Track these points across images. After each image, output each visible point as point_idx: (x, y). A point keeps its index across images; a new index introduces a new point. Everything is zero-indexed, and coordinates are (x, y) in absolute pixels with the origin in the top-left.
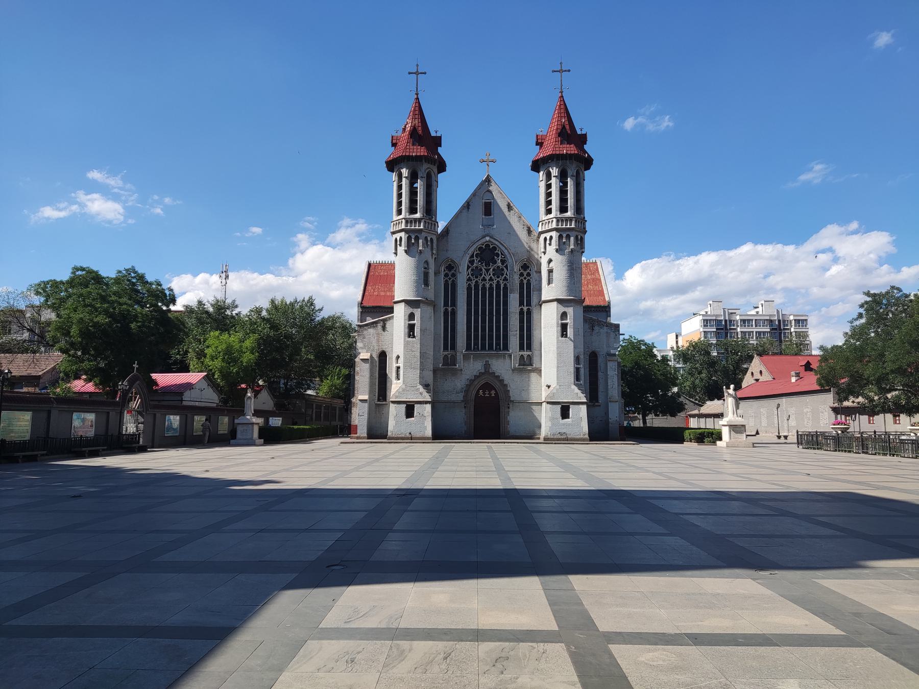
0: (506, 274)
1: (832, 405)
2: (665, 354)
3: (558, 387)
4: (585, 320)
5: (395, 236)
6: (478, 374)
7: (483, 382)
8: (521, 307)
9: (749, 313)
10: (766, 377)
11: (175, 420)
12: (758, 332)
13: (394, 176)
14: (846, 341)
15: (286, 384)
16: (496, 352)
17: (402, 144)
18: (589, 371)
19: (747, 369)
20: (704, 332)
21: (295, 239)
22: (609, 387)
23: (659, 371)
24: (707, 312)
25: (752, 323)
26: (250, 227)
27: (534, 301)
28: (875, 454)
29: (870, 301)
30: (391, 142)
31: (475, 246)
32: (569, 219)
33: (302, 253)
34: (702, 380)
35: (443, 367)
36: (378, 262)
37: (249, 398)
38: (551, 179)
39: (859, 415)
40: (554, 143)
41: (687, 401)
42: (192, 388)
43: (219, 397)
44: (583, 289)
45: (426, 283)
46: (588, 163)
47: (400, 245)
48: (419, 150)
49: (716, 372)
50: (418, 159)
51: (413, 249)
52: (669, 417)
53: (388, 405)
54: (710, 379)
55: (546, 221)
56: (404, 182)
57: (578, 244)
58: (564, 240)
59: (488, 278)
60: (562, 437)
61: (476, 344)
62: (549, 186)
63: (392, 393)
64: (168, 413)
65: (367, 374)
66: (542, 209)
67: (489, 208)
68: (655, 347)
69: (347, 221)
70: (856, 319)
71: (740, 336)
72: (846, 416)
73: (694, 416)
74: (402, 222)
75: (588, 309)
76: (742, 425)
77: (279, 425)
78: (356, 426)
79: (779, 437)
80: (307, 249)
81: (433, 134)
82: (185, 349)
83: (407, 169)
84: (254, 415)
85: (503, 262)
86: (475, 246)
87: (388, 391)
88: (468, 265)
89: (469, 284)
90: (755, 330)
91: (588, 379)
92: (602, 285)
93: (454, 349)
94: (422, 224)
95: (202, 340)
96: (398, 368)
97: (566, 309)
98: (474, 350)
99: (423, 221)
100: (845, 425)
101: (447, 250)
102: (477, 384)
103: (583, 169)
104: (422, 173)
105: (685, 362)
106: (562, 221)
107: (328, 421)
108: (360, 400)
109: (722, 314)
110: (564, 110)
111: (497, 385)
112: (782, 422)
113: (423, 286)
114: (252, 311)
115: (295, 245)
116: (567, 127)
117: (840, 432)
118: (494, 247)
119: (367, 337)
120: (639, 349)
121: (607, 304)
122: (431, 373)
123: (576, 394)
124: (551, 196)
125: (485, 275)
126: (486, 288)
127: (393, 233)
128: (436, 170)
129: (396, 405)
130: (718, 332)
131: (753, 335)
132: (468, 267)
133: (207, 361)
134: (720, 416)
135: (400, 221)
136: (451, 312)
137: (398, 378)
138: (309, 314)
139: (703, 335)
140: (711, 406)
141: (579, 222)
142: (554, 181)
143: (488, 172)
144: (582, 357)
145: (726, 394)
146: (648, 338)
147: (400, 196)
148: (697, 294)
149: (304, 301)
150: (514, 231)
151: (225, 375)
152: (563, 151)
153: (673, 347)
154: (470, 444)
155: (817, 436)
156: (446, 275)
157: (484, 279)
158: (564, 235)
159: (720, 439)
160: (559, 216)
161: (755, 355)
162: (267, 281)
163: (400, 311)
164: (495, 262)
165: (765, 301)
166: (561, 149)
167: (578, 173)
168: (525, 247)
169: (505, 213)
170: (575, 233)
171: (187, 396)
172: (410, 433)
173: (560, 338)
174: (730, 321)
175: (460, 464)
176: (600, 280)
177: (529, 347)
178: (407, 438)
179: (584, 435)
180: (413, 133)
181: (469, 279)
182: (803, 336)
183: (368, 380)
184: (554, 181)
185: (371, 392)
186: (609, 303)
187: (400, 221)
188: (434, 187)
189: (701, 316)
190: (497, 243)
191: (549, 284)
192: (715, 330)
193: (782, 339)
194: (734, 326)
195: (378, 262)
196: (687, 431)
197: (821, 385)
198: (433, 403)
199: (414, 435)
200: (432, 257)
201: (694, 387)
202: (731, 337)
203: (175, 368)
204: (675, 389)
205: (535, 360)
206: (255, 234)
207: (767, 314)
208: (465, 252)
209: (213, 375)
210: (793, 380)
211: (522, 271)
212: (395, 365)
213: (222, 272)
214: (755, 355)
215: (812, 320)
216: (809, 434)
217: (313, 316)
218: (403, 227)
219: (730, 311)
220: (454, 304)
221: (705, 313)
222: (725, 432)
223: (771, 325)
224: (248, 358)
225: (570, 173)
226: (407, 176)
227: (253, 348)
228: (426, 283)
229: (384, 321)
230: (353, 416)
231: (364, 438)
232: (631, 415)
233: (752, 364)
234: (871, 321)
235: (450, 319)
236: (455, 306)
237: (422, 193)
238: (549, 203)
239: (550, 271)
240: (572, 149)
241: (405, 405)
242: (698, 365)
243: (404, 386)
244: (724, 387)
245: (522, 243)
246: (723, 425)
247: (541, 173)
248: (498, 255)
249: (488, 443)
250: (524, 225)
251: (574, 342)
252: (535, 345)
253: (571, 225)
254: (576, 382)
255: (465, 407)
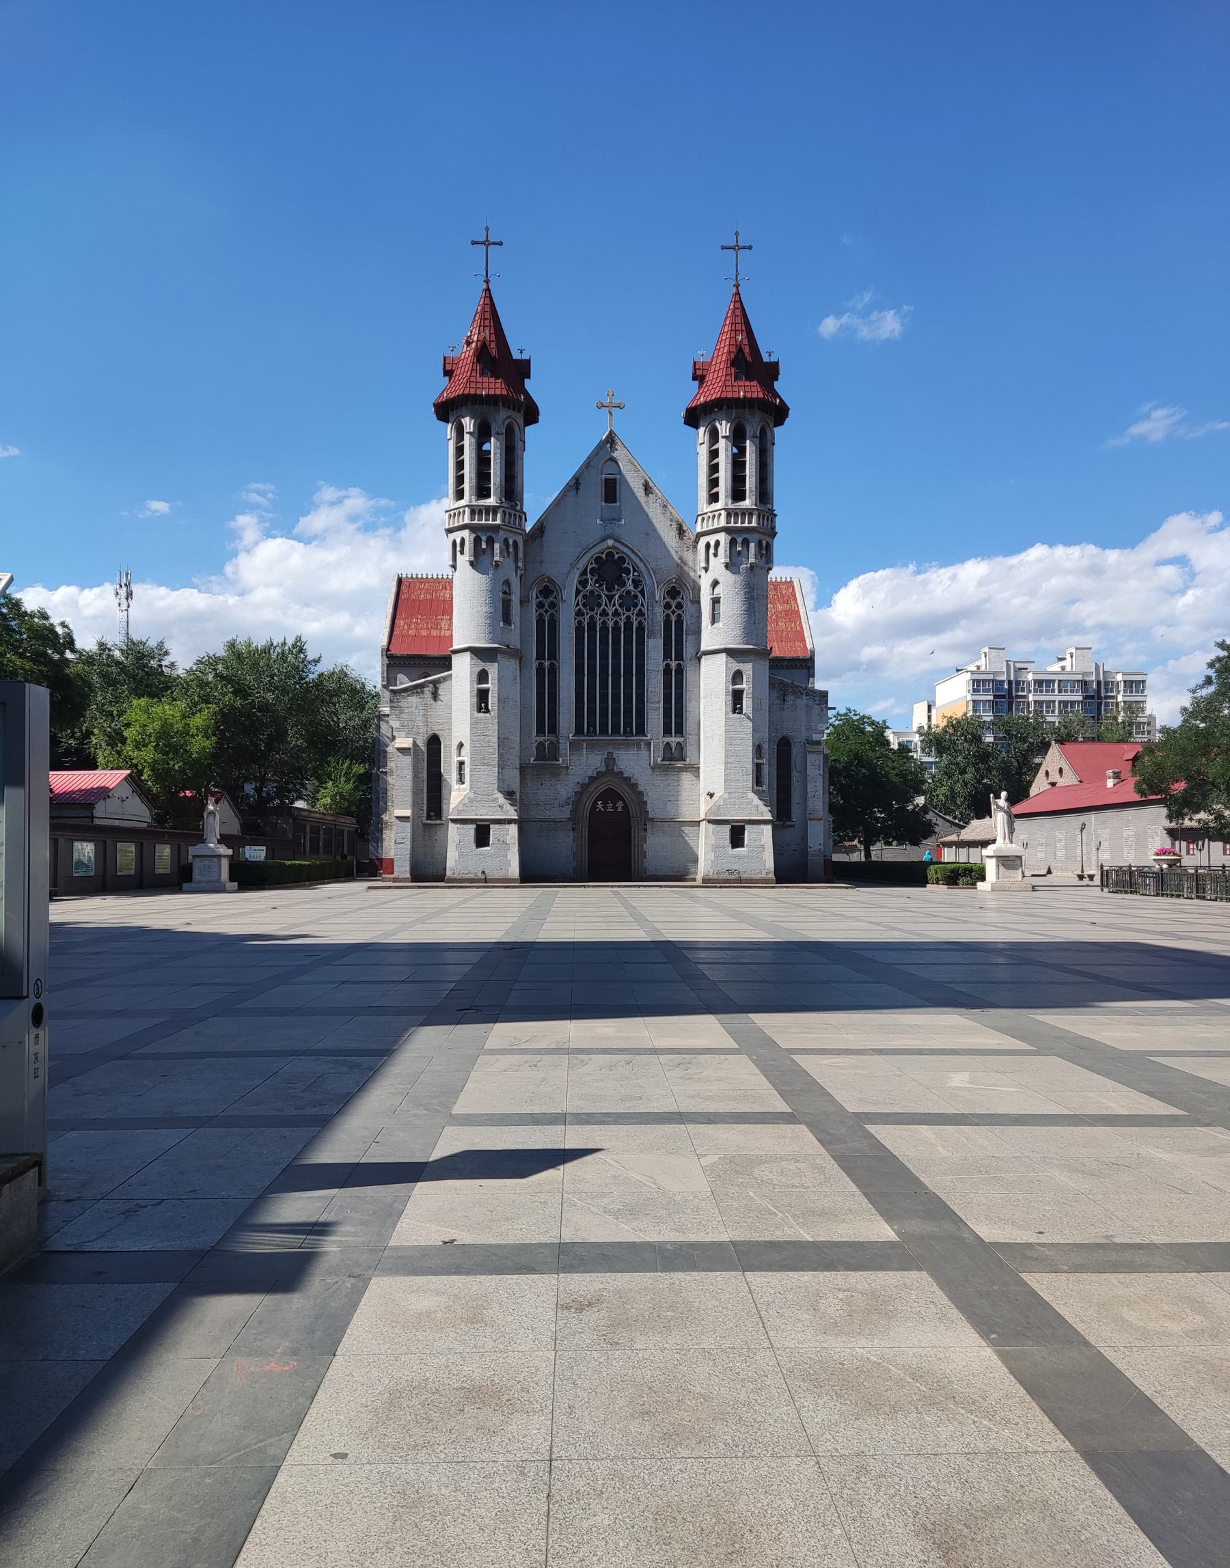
0: (642, 605)
1: (1167, 824)
2: (905, 739)
3: (726, 796)
4: (772, 684)
5: (453, 536)
6: (595, 775)
7: (603, 788)
8: (666, 662)
9: (1050, 669)
10: (1069, 779)
11: (85, 850)
12: (1064, 701)
13: (449, 430)
14: (1184, 721)
15: (258, 791)
16: (624, 738)
17: (463, 372)
18: (777, 769)
19: (1040, 765)
20: (974, 701)
21: (232, 524)
22: (809, 796)
23: (893, 769)
24: (978, 667)
25: (1054, 686)
26: (146, 500)
27: (688, 651)
28: (1216, 900)
29: (1224, 657)
30: (442, 367)
31: (589, 555)
32: (747, 513)
33: (248, 551)
34: (966, 784)
35: (535, 762)
36: (414, 576)
37: (212, 813)
38: (718, 442)
39: (1209, 840)
40: (723, 379)
41: (939, 819)
42: (109, 797)
43: (151, 812)
44: (769, 628)
45: (507, 619)
46: (780, 413)
47: (462, 552)
48: (492, 385)
49: (989, 769)
50: (492, 400)
51: (485, 559)
52: (909, 847)
53: (445, 826)
54: (979, 782)
55: (710, 514)
56: (467, 441)
57: (761, 555)
58: (739, 549)
59: (611, 611)
60: (732, 877)
61: (592, 724)
62: (714, 454)
63: (452, 807)
64: (76, 838)
65: (408, 774)
66: (703, 494)
67: (612, 489)
68: (888, 728)
69: (329, 493)
70: (1202, 687)
71: (1032, 709)
72: (1189, 843)
73: (949, 845)
74: (464, 512)
75: (778, 664)
76: (1017, 857)
77: (262, 859)
78: (392, 861)
79: (1081, 877)
80: (256, 543)
81: (516, 355)
82: (84, 728)
83: (472, 418)
84: (219, 842)
85: (636, 583)
86: (589, 555)
87: (444, 802)
88: (577, 588)
89: (580, 621)
90: (1058, 699)
91: (775, 783)
92: (800, 622)
93: (555, 733)
94: (499, 515)
95: (115, 713)
96: (461, 763)
97: (740, 666)
98: (588, 735)
99: (501, 510)
100: (1175, 855)
101: (541, 562)
102: (594, 791)
103: (772, 425)
104: (499, 427)
105: (940, 753)
106: (736, 515)
107: (331, 854)
108: (397, 817)
109: (1005, 670)
110: (741, 319)
111: (626, 792)
112: (1089, 854)
113: (502, 624)
114: (201, 662)
115: (235, 535)
116: (747, 350)
117: (1165, 866)
118: (623, 557)
119: (406, 710)
120: (863, 731)
121: (808, 656)
122: (517, 772)
123: (756, 808)
124: (717, 471)
125: (606, 605)
126: (608, 628)
127: (449, 531)
128: (521, 422)
129: (458, 826)
130: (997, 702)
131: (1054, 707)
132: (578, 592)
133: (128, 749)
134: (984, 844)
135: (461, 510)
136: (548, 670)
137: (461, 780)
138: (298, 667)
139: (971, 708)
140: (976, 829)
141: (764, 516)
142: (722, 445)
143: (611, 425)
144: (765, 746)
145: (993, 807)
146: (875, 710)
147: (460, 465)
148: (959, 635)
149: (284, 644)
150: (655, 530)
151: (161, 775)
152: (739, 392)
153: (922, 727)
154: (582, 889)
155: (1131, 873)
156: (540, 605)
157: (604, 613)
158: (740, 540)
159: (983, 878)
160: (730, 506)
161: (1053, 743)
162: (191, 599)
163: (463, 668)
164: (623, 584)
165: (1077, 649)
166: (736, 389)
167: (763, 431)
168: (674, 559)
169: (639, 498)
170: (756, 537)
171: (101, 810)
172: (483, 872)
173: (731, 715)
174: (1018, 683)
175: (578, 914)
176: (798, 613)
177: (680, 730)
178: (479, 881)
179: (767, 873)
180: (482, 354)
181: (579, 613)
182: (1134, 708)
183: (410, 784)
184: (722, 445)
185: (415, 804)
186: (813, 653)
187: (461, 510)
188: (518, 452)
189: (969, 674)
190: (626, 550)
191: (713, 622)
192: (991, 698)
193: (1103, 713)
194: (1023, 691)
195: (414, 576)
196: (932, 867)
197: (1142, 792)
198: (521, 823)
199: (490, 875)
200: (516, 573)
201: (953, 796)
202: (1017, 709)
203: (67, 762)
204: (921, 800)
205: (690, 751)
206: (157, 514)
207: (1079, 670)
208: (573, 566)
209: (140, 773)
210: (1110, 783)
211: (668, 600)
212: (455, 759)
213: (121, 586)
214: (1053, 743)
215: (1151, 680)
216: (1119, 870)
217: (303, 671)
218: (467, 520)
219: (1018, 665)
220: (554, 655)
221: (975, 669)
222: (991, 867)
223: (1085, 690)
224: (200, 745)
225: (749, 430)
226: (472, 430)
227: (208, 728)
228: (507, 619)
229: (435, 683)
230: (385, 844)
231: (404, 880)
232: (847, 844)
233: (1047, 757)
234: (1224, 690)
235: (547, 679)
236: (556, 659)
237: (499, 461)
238: (714, 483)
239: (716, 601)
240: (754, 389)
241: (475, 826)
242: (960, 759)
243: (472, 795)
244: (992, 795)
245: (669, 551)
246: (987, 857)
247: (702, 430)
248: (628, 572)
249: (612, 886)
250: (671, 520)
251: (753, 721)
252: (689, 726)
253: (750, 522)
254: (756, 788)
255: (573, 829)
